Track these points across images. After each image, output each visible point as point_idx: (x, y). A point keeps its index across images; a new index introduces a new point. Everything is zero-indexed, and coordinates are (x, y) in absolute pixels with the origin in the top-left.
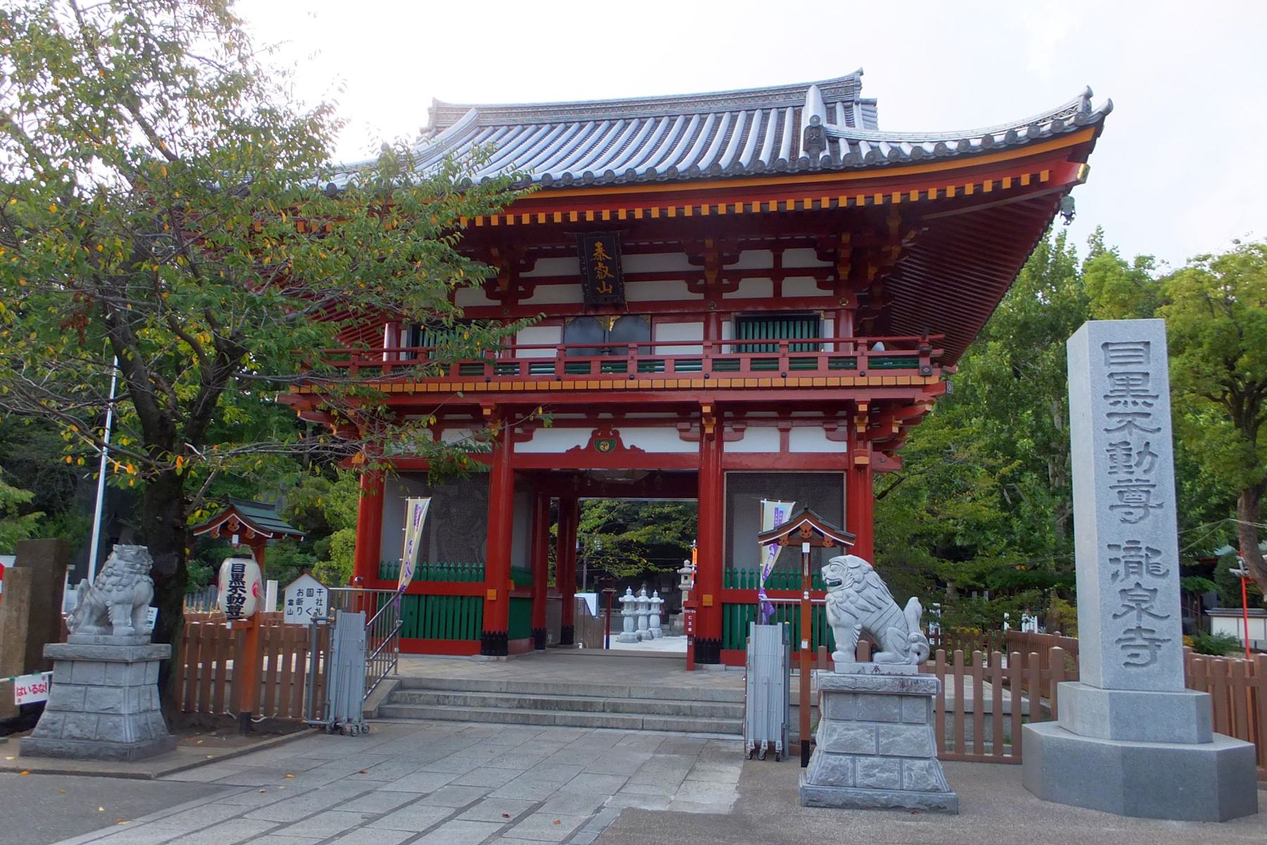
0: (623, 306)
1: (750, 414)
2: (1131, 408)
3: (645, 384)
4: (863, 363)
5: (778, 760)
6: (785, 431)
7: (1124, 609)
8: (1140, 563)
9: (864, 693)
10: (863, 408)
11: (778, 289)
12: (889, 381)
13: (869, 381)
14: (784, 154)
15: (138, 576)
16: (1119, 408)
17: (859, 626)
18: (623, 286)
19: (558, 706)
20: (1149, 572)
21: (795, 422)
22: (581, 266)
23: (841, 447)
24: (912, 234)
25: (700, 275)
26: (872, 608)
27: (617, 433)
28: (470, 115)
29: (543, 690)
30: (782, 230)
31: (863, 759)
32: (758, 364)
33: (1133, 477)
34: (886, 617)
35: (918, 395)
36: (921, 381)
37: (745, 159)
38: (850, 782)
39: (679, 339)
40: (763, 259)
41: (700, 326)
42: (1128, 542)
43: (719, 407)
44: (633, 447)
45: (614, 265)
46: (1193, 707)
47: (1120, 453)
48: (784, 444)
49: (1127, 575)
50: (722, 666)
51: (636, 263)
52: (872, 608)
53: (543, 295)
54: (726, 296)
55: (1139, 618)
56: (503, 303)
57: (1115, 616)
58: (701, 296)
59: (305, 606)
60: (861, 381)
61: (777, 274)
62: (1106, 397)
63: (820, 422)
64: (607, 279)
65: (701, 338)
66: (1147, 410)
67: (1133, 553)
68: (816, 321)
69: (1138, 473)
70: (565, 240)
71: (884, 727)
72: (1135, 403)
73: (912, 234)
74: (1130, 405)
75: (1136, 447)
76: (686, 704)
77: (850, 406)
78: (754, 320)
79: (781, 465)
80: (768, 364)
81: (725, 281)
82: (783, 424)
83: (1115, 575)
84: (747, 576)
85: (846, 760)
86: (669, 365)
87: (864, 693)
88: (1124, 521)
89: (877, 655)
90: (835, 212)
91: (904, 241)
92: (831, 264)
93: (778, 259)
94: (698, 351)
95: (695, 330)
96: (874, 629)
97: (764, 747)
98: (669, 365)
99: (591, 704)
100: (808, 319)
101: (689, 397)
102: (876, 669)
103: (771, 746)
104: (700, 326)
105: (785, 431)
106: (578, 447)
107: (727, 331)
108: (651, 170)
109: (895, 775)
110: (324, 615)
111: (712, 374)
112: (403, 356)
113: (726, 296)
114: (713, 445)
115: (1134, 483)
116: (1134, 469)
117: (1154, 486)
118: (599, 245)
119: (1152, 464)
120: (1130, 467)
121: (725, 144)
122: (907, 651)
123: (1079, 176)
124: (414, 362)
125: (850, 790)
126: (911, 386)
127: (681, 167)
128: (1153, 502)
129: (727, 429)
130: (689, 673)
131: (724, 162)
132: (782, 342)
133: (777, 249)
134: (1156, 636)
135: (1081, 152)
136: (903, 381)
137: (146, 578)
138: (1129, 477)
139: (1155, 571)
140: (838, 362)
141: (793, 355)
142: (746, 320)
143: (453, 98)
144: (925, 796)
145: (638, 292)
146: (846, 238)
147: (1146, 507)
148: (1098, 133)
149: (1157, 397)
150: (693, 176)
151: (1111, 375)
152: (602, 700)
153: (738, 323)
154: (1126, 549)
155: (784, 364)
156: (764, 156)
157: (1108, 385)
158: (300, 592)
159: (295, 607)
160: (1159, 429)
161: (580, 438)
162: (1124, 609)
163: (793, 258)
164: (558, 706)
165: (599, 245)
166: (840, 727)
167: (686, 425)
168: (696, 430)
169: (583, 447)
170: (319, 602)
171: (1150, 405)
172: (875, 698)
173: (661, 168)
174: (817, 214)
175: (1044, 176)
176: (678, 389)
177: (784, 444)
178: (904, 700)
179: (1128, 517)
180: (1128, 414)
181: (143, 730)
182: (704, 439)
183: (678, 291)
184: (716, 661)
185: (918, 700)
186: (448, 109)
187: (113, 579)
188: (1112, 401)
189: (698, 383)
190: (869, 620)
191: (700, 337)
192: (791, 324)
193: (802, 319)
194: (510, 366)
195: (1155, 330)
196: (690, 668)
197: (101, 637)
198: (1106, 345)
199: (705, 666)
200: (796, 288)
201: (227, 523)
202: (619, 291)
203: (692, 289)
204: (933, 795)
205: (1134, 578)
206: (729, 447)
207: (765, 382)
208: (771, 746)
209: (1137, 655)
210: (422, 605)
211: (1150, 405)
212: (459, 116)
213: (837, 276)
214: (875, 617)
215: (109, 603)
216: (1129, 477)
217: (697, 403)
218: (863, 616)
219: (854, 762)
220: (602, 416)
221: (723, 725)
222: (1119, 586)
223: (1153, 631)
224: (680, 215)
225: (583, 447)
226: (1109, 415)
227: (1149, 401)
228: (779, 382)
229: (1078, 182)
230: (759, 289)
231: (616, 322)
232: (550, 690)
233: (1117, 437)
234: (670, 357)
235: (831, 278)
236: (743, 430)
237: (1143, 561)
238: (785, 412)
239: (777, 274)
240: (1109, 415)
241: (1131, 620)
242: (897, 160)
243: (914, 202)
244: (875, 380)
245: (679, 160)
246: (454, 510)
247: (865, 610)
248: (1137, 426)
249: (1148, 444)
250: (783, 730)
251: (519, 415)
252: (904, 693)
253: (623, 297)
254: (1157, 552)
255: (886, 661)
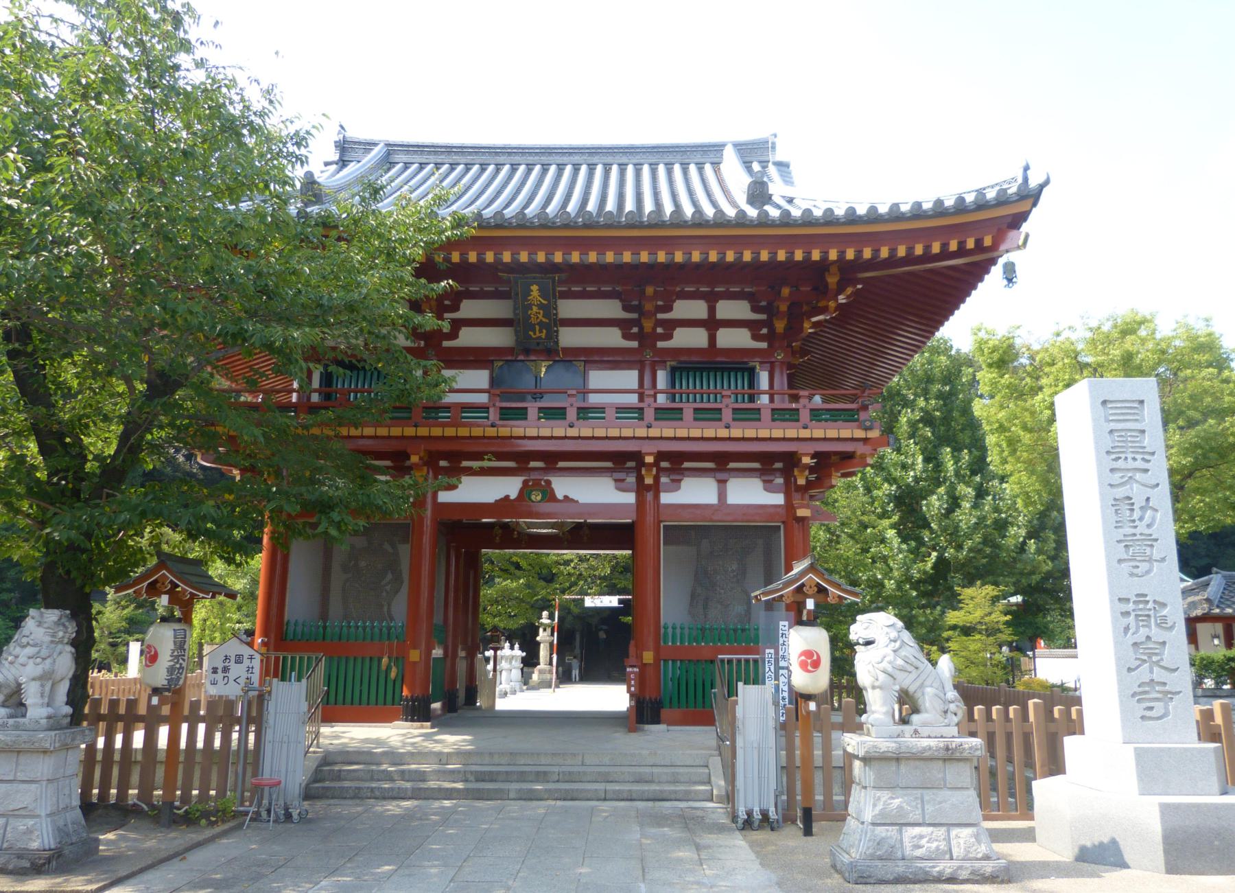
0: (556, 352)
1: (686, 465)
2: (1131, 464)
3: (504, 432)
4: (805, 415)
5: (772, 829)
6: (722, 483)
7: (1138, 662)
8: (1148, 616)
9: (908, 759)
10: (649, 459)
11: (712, 339)
12: (832, 434)
13: (809, 433)
14: (591, 206)
15: (60, 646)
16: (1120, 464)
17: (897, 688)
18: (557, 332)
19: (508, 777)
20: (1158, 625)
21: (732, 474)
22: (515, 309)
23: (778, 499)
24: (849, 290)
25: (636, 322)
26: (910, 668)
27: (549, 483)
28: (377, 152)
29: (487, 760)
30: (712, 280)
31: (909, 829)
32: (702, 415)
33: (1137, 531)
34: (923, 677)
35: (860, 449)
36: (860, 434)
37: (572, 208)
38: (899, 854)
39: (614, 385)
40: (698, 309)
41: (634, 374)
42: (1137, 595)
43: (661, 456)
44: (566, 497)
45: (549, 309)
46: (1212, 759)
47: (1124, 508)
48: (722, 495)
49: (1138, 628)
50: (662, 727)
51: (569, 308)
52: (910, 668)
53: (469, 338)
54: (660, 344)
55: (1151, 671)
56: (770, 346)
57: (1129, 670)
58: (635, 344)
59: (232, 675)
60: (805, 434)
61: (712, 324)
62: (1108, 452)
63: (758, 474)
64: (541, 324)
65: (635, 386)
66: (1146, 466)
67: (1141, 606)
68: (752, 374)
69: (1142, 528)
70: (541, 282)
71: (928, 795)
72: (1134, 459)
73: (849, 290)
74: (1129, 460)
75: (1139, 502)
76: (648, 770)
77: (637, 456)
78: (688, 370)
79: (721, 520)
80: (713, 415)
81: (659, 330)
82: (721, 476)
83: (1127, 629)
84: (678, 631)
85: (892, 831)
86: (610, 414)
87: (908, 759)
88: (1132, 575)
89: (915, 718)
90: (773, 264)
91: (840, 297)
92: (634, 316)
93: (712, 310)
94: (483, 398)
95: (629, 378)
96: (911, 690)
97: (757, 816)
98: (610, 414)
99: (545, 773)
100: (743, 370)
101: (848, 447)
102: (916, 732)
103: (765, 815)
104: (634, 374)
105: (722, 483)
106: (507, 497)
107: (662, 378)
108: (499, 213)
109: (943, 845)
110: (256, 685)
111: (654, 423)
112: (315, 398)
113: (660, 344)
114: (649, 496)
115: (1138, 537)
116: (1137, 523)
117: (1156, 540)
118: (535, 288)
119: (1154, 519)
120: (1134, 521)
121: (499, 193)
122: (946, 712)
123: (1021, 242)
124: (327, 403)
125: (901, 863)
126: (852, 439)
127: (509, 212)
128: (1156, 556)
129: (664, 480)
130: (633, 735)
131: (551, 209)
132: (724, 393)
133: (712, 300)
134: (1167, 688)
135: (1017, 220)
136: (846, 434)
137: (69, 649)
138: (1133, 531)
139: (1163, 624)
140: (780, 415)
141: (737, 406)
142: (681, 369)
143: (356, 132)
144: (977, 865)
145: (569, 338)
146: (786, 291)
147: (1150, 560)
148: (1035, 205)
149: (1153, 454)
150: (522, 222)
151: (1111, 432)
152: (556, 769)
153: (673, 372)
154: (1135, 602)
155: (727, 415)
156: (591, 206)
157: (1108, 442)
158: (226, 658)
159: (220, 675)
160: (1158, 485)
161: (510, 487)
162: (1138, 662)
163: (726, 309)
164: (508, 777)
165: (535, 288)
166: (885, 795)
167: (621, 475)
168: (631, 479)
169: (513, 496)
170: (250, 669)
171: (1149, 461)
172: (918, 763)
173: (488, 213)
174: (756, 265)
175: (988, 241)
176: (538, 438)
177: (722, 495)
178: (948, 765)
179: (1135, 571)
180: (1128, 470)
181: (61, 832)
182: (641, 489)
183: (612, 338)
184: (657, 721)
185: (961, 764)
186: (355, 143)
187: (30, 651)
188: (1114, 456)
189: (641, 432)
190: (907, 681)
191: (485, 384)
192: (726, 375)
193: (736, 370)
194: (434, 409)
195: (1147, 388)
196: (632, 730)
197: (11, 721)
198: (1104, 402)
199: (647, 727)
200: (729, 339)
201: (156, 581)
202: (553, 336)
203: (626, 336)
204: (984, 863)
205: (1143, 632)
206: (666, 498)
207: (709, 433)
208: (765, 815)
209: (1151, 708)
210: (342, 668)
211: (1149, 461)
212: (368, 151)
213: (641, 328)
214: (913, 676)
215: (23, 680)
216: (1133, 531)
217: (640, 452)
218: (900, 676)
219: (900, 832)
220: (533, 464)
221: (622, 791)
222: (1130, 639)
223: (1165, 684)
224: (481, 260)
225: (513, 496)
226: (1112, 470)
227: (1147, 457)
228: (723, 433)
229: (1019, 248)
230: (694, 338)
231: (548, 368)
232: (496, 760)
233: (1121, 492)
234: (611, 405)
235: (635, 330)
236: (679, 481)
237: (1152, 613)
238: (721, 463)
239: (712, 324)
240: (1112, 470)
241: (1143, 674)
242: (808, 220)
243: (798, 262)
244: (819, 433)
245: (507, 206)
246: (363, 564)
247: (902, 670)
248: (1137, 482)
249: (1148, 499)
250: (776, 796)
251: (453, 459)
252: (949, 756)
253: (557, 343)
254: (1164, 605)
255: (924, 725)
